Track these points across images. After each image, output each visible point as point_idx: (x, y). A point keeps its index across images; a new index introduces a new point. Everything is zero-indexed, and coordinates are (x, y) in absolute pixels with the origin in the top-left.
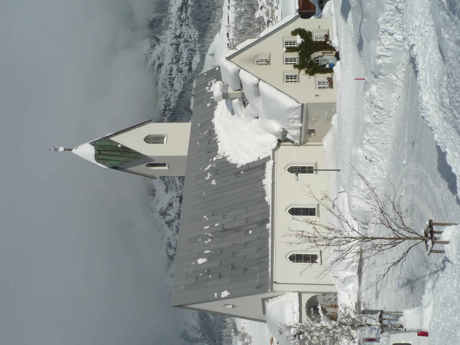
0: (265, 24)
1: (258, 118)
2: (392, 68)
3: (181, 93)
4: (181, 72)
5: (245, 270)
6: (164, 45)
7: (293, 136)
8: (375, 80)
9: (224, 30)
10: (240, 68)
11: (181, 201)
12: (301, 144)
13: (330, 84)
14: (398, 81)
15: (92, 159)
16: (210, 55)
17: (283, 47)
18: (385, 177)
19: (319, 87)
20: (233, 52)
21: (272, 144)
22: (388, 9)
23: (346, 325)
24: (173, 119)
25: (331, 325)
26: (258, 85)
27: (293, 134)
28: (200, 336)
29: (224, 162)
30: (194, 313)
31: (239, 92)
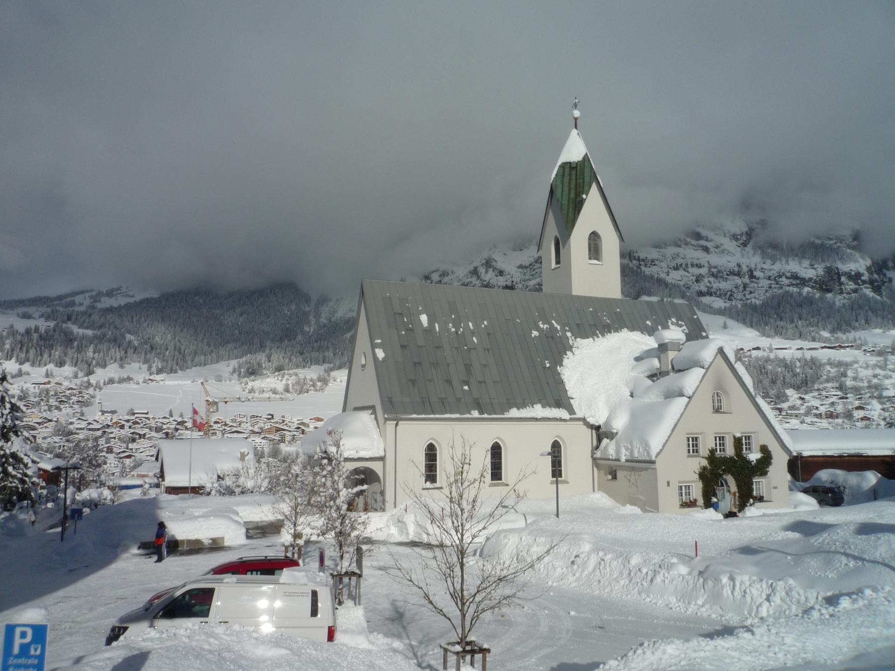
0: (776, 404)
1: (632, 396)
2: (715, 598)
3: (664, 282)
4: (697, 281)
5: (413, 382)
6: (738, 254)
7: (605, 448)
8: (696, 572)
9: (764, 342)
10: (707, 369)
12: (594, 459)
13: (686, 503)
15: (563, 159)
18: (550, 583)
19: (681, 487)
21: (593, 417)
22: (809, 594)
23: (341, 524)
24: (625, 271)
26: (681, 395)
27: (610, 447)
28: (323, 320)
31: (670, 367)
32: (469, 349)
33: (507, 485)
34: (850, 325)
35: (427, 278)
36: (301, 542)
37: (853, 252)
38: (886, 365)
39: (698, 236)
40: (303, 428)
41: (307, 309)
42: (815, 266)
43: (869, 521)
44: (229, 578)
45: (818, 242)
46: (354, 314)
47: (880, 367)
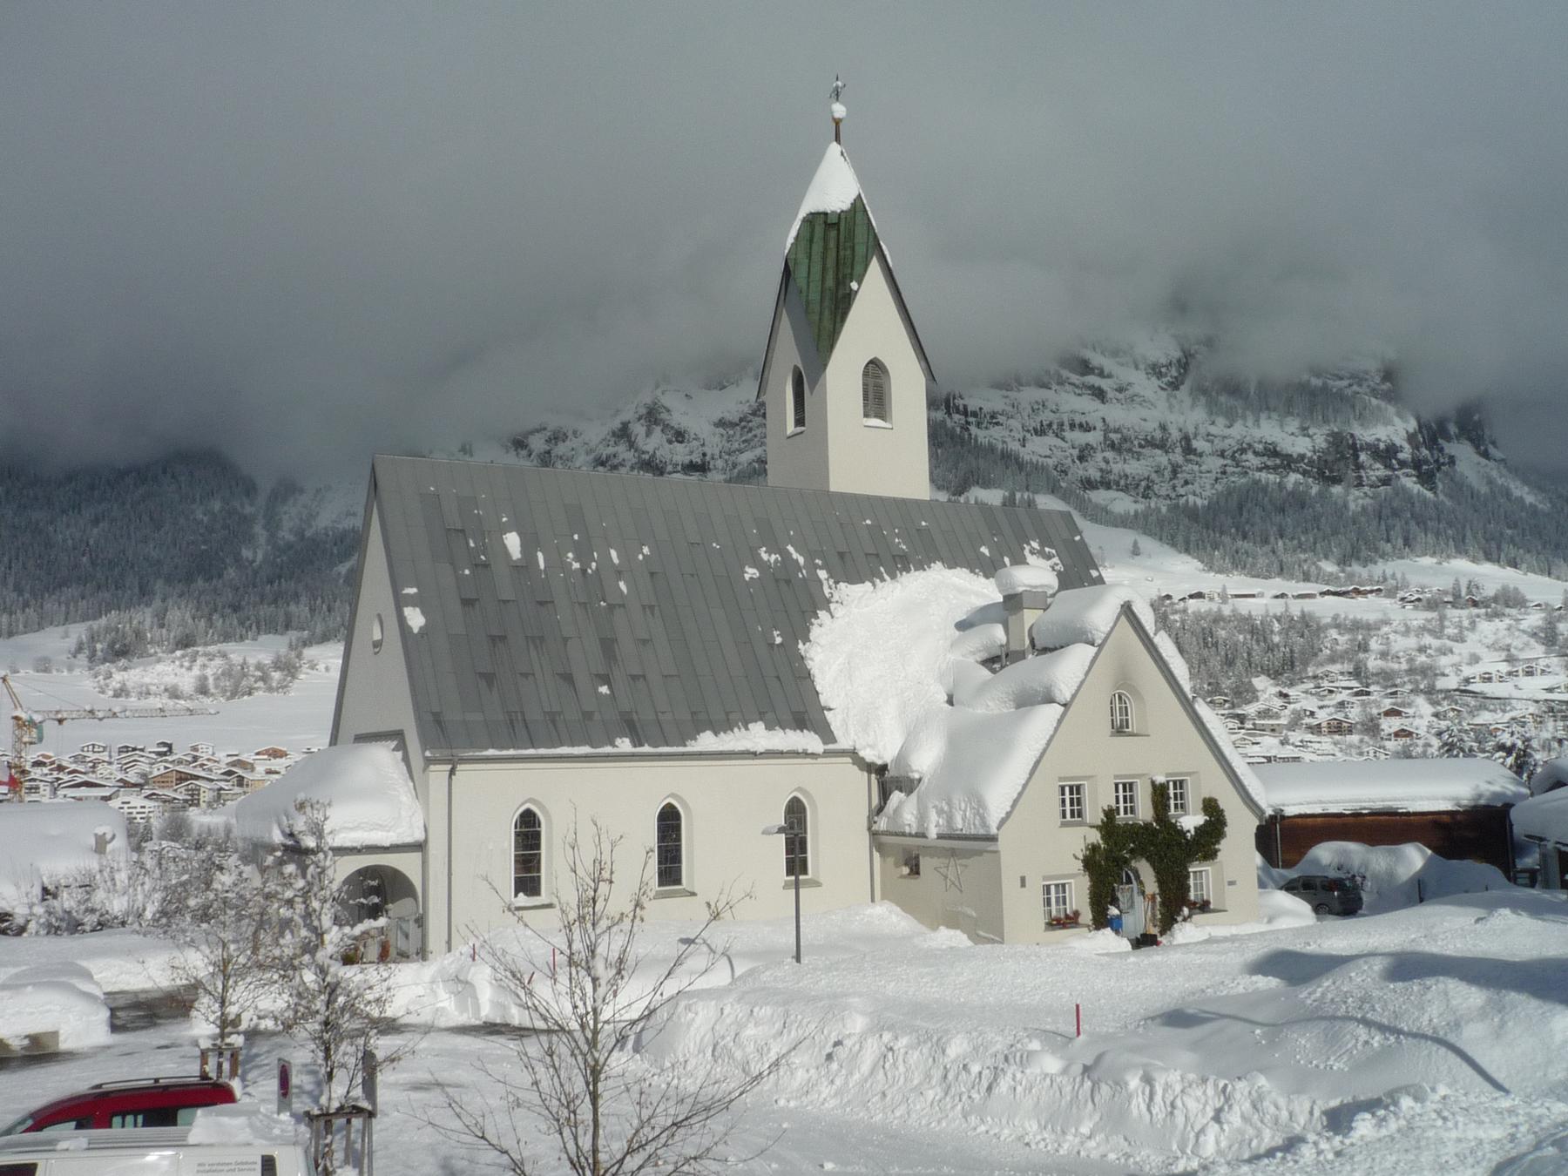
0: (1233, 706)
1: (950, 702)
2: (1116, 1119)
3: (1016, 459)
4: (1081, 458)
5: (489, 678)
6: (1162, 404)
7: (897, 811)
8: (1077, 1069)
9: (1212, 582)
10: (1101, 646)
11: (691, 468)
12: (874, 835)
13: (1058, 920)
14: (1077, 1140)
15: (810, 205)
16: (1135, 544)
17: (1168, 775)
18: (782, 1103)
19: (1048, 887)
20: (1148, 619)
21: (872, 747)
22: (1296, 1107)
23: (328, 1003)
24: (938, 437)
25: (327, 961)
26: (1049, 699)
27: (905, 810)
28: (286, 535)
29: (811, 604)
30: (354, 514)
31: (1027, 642)
32: (611, 607)
33: (693, 894)
34: (1376, 550)
35: (520, 444)
36: (237, 1040)
37: (1383, 404)
38: (1443, 627)
39: (1085, 368)
40: (240, 772)
41: (248, 510)
42: (1311, 432)
43: (1408, 947)
44: (68, 1137)
45: (1316, 382)
46: (358, 522)
47: (1432, 632)
